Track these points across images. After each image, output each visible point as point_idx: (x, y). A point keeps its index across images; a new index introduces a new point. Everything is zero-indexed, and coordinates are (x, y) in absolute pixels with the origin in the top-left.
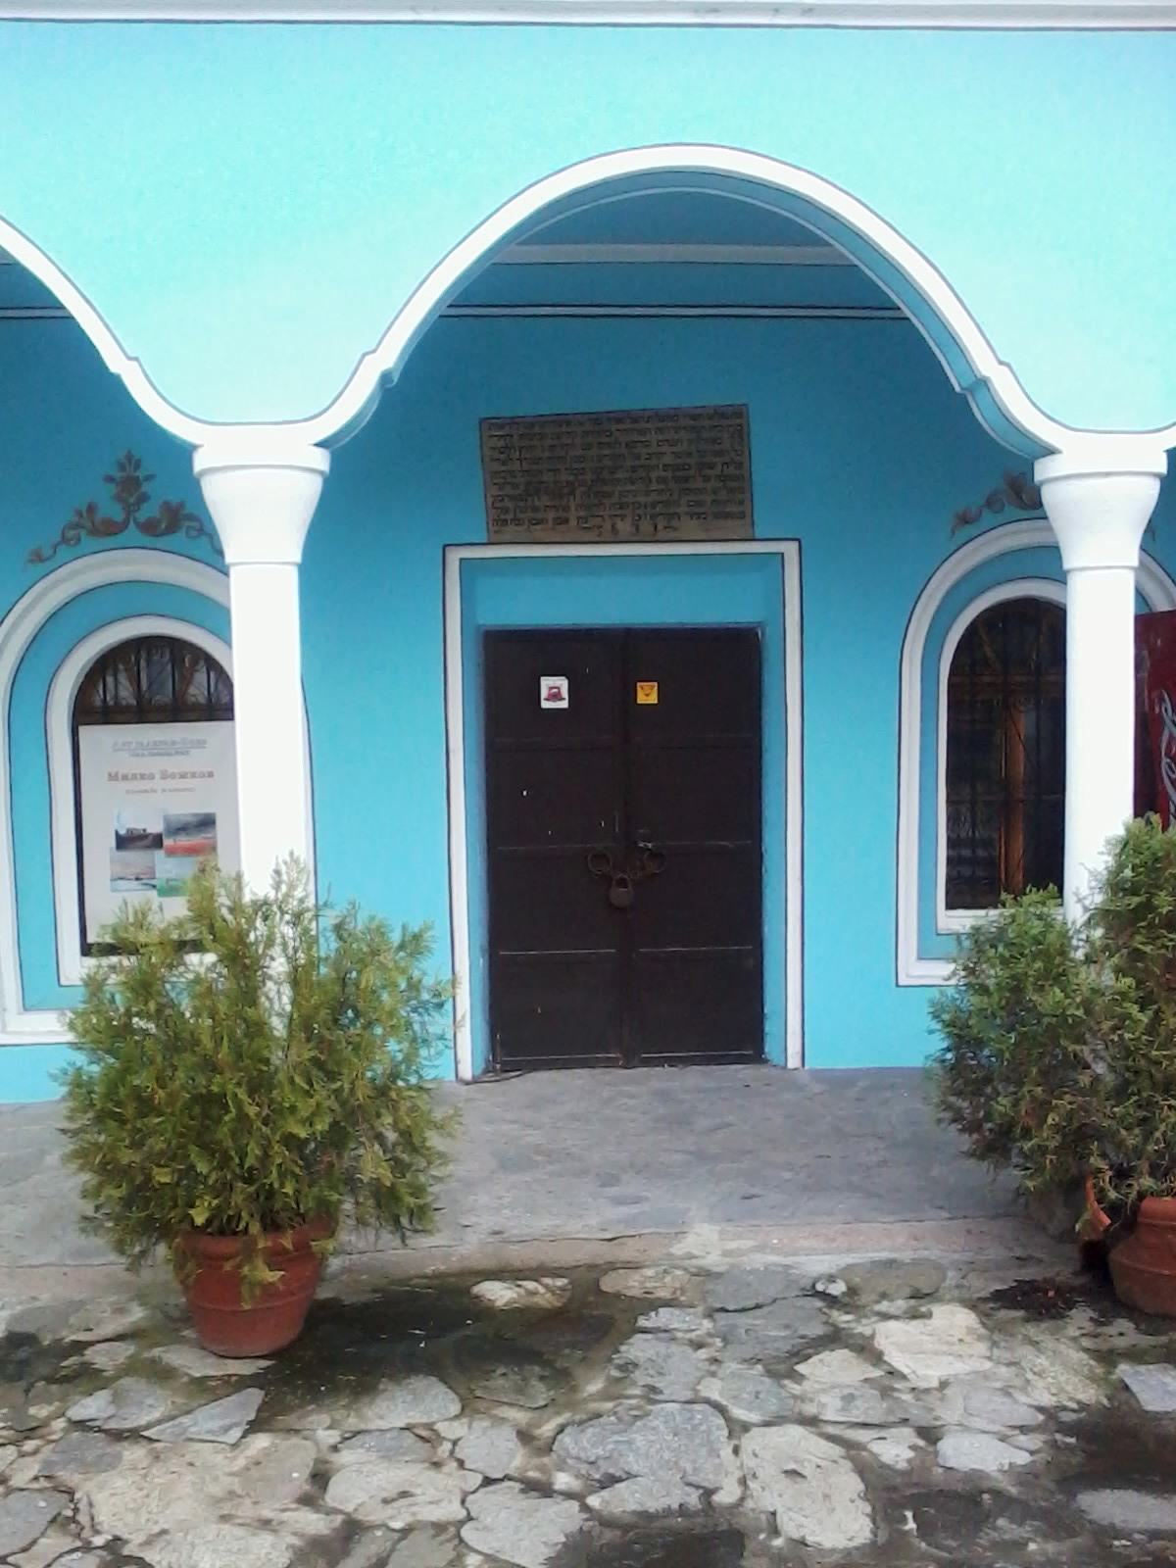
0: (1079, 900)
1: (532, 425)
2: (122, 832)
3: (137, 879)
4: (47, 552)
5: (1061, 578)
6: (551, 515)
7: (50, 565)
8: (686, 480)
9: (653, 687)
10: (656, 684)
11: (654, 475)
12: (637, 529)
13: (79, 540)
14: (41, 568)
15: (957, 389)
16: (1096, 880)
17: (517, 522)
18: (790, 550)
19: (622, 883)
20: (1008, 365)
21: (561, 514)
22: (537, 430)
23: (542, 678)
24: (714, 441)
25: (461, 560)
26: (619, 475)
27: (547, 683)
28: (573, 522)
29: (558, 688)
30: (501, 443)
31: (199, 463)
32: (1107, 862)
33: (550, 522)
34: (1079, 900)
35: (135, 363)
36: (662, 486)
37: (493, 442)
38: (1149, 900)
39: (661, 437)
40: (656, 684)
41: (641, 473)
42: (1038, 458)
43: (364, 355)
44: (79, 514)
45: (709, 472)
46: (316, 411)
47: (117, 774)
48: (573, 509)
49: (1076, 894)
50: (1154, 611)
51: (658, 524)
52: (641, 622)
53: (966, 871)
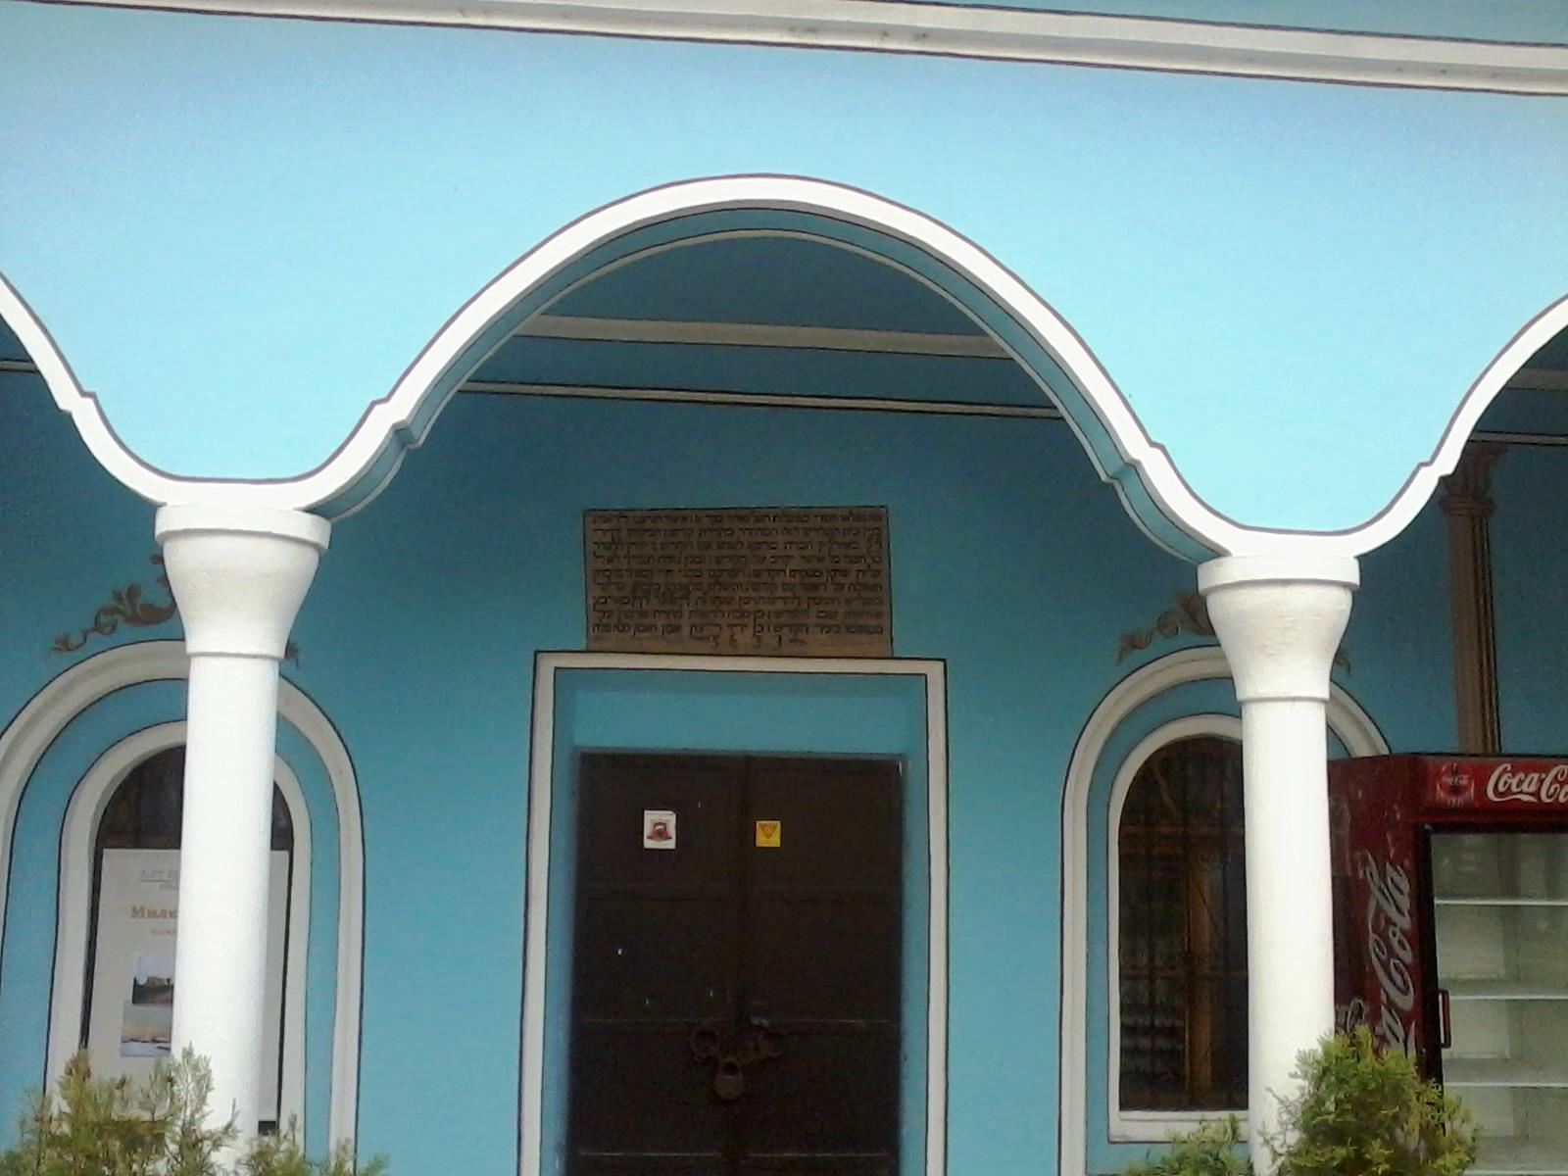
0: (1266, 1142)
1: (643, 519)
2: (142, 981)
3: (154, 1041)
4: (76, 639)
5: (1235, 711)
6: (661, 622)
7: (79, 654)
8: (816, 587)
9: (775, 827)
10: (778, 823)
11: (779, 580)
12: (759, 639)
13: (114, 629)
14: (68, 657)
15: (1104, 477)
16: (1289, 1112)
17: (622, 628)
18: (933, 671)
19: (731, 1069)
20: (1162, 448)
21: (673, 621)
22: (648, 524)
23: (646, 812)
24: (847, 545)
25: (556, 668)
26: (740, 579)
27: (651, 817)
28: (686, 631)
29: (664, 824)
30: (607, 538)
31: (164, 524)
32: (1302, 1088)
33: (660, 629)
34: (1266, 1142)
35: (90, 401)
36: (789, 594)
37: (599, 536)
38: (1359, 1155)
39: (789, 538)
40: (778, 823)
41: (765, 577)
42: (1200, 563)
43: (374, 404)
44: (118, 597)
45: (842, 580)
46: (311, 468)
47: (142, 909)
48: (687, 615)
49: (1262, 1133)
50: (1353, 756)
51: (784, 634)
52: (724, 747)
53: (1144, 1064)
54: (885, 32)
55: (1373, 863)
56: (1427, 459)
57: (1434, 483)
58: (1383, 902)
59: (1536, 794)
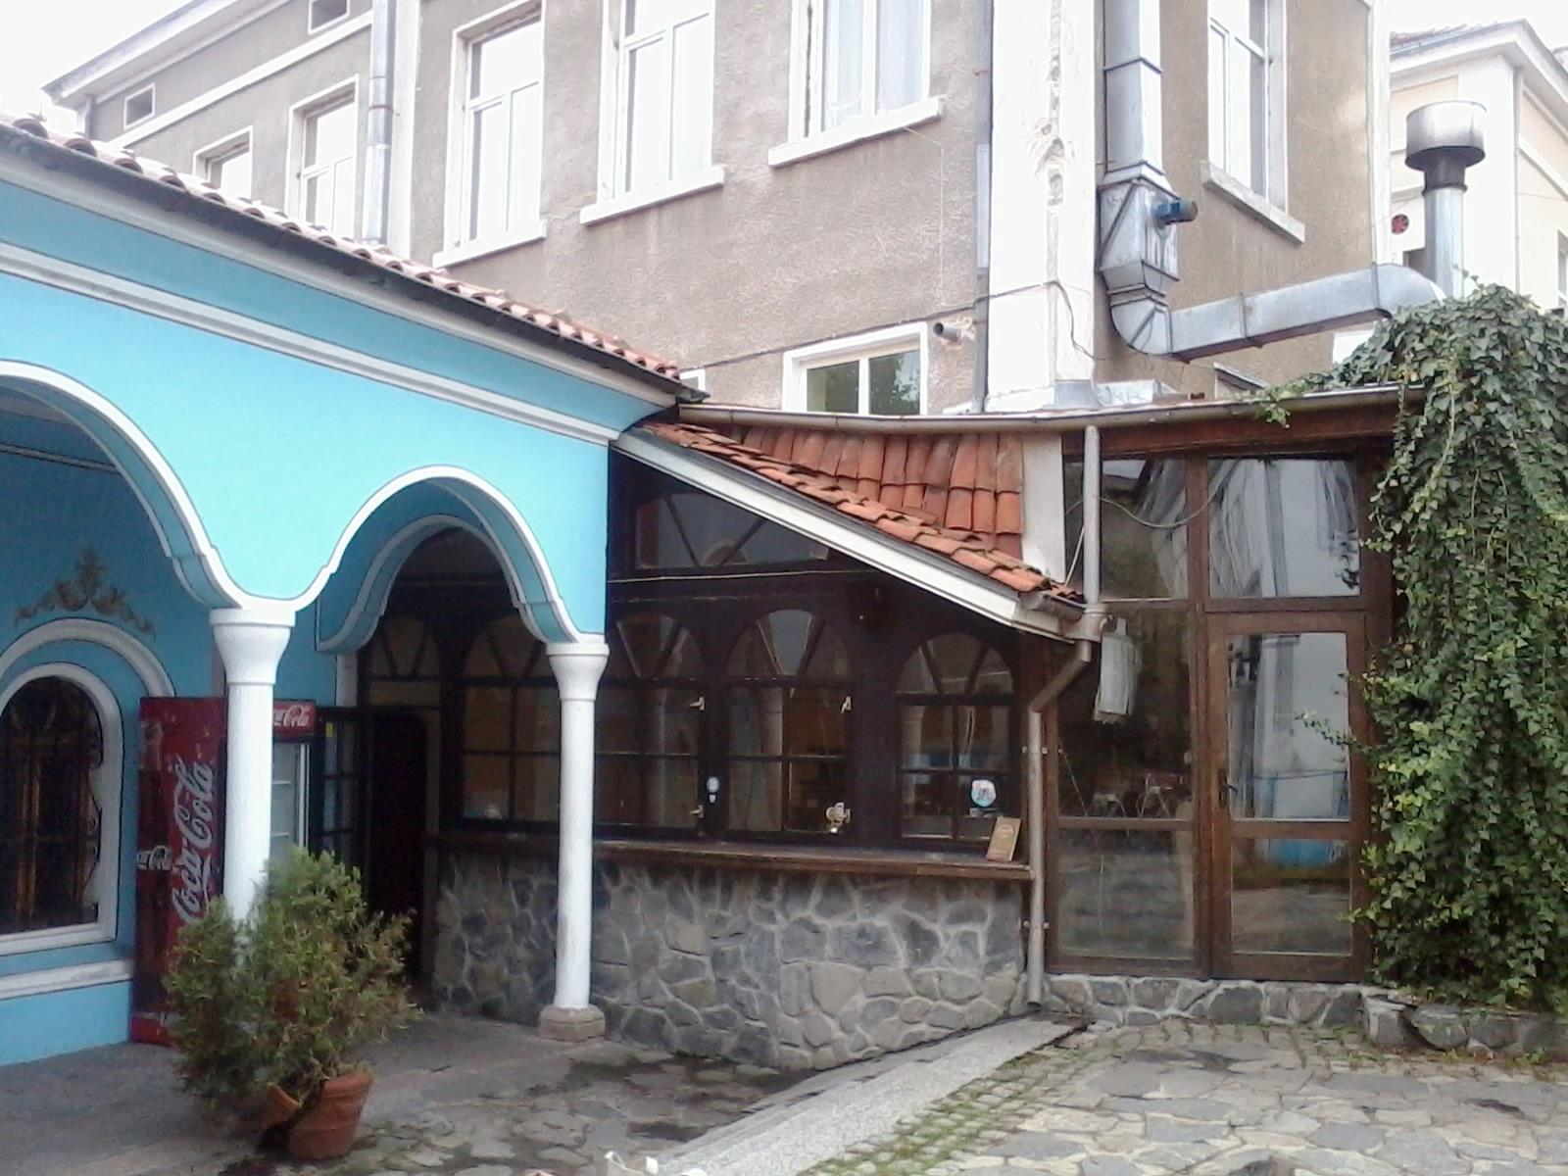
54: (94, 287)
55: (181, 762)
56: (325, 563)
57: (328, 577)
58: (188, 784)
59: (282, 722)
